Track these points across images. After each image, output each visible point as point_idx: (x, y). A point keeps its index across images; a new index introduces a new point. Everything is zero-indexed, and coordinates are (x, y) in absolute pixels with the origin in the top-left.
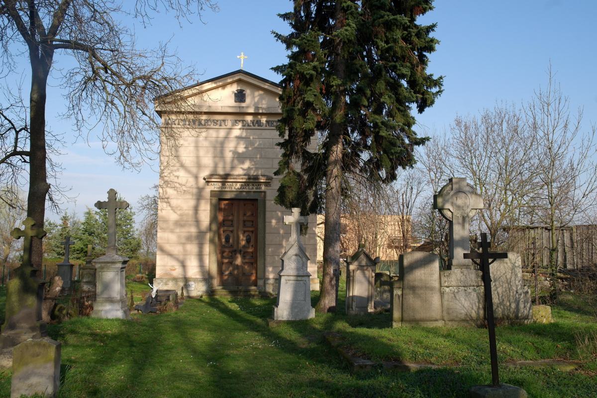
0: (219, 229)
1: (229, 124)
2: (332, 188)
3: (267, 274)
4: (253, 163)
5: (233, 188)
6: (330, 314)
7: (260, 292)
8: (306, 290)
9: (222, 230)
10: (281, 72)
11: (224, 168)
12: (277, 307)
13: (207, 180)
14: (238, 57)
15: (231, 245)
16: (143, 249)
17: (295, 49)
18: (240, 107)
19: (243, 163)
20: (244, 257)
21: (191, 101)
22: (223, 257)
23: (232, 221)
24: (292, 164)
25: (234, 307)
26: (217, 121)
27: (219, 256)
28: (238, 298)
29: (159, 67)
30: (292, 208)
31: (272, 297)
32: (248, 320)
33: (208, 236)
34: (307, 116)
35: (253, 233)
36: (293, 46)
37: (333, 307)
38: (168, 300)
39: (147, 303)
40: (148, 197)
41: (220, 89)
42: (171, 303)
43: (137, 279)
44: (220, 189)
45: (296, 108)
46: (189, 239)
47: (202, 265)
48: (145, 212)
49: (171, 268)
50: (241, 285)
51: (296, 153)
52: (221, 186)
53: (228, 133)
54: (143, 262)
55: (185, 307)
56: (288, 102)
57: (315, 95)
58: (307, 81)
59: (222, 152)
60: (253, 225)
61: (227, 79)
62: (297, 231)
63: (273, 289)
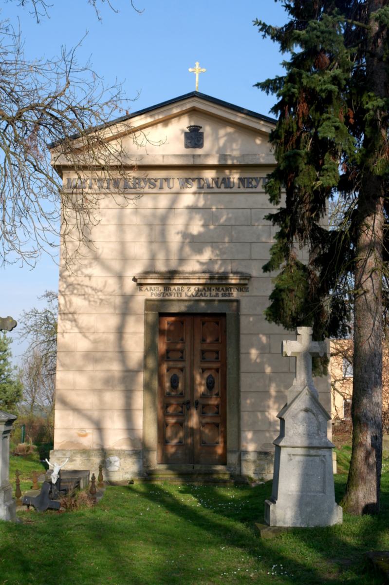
0: (159, 365)
1: (176, 185)
2: (365, 292)
3: (244, 443)
4: (218, 252)
5: (183, 294)
6: (368, 517)
7: (232, 476)
8: (324, 475)
9: (164, 367)
10: (274, 90)
11: (167, 260)
12: (275, 503)
13: (139, 281)
14: (190, 70)
15: (181, 394)
16: (26, 400)
17: (298, 49)
18: (194, 156)
19: (200, 251)
20: (202, 414)
21: (114, 146)
22: (166, 414)
23: (182, 352)
24: (295, 250)
25: (190, 500)
26: (156, 180)
27: (161, 413)
28: (194, 486)
29: (62, 89)
30: (298, 328)
31: (253, 485)
32: (220, 526)
33: (141, 377)
34: (323, 164)
36: (293, 45)
37: (373, 504)
38: (78, 487)
39: (43, 494)
40: (35, 313)
41: (160, 125)
42: (83, 493)
43: (20, 451)
44: (161, 297)
45: (303, 152)
46: (108, 383)
47: (130, 429)
48: (31, 337)
49: (80, 432)
50: (198, 463)
51: (301, 231)
52: (162, 291)
53: (174, 202)
54: (26, 422)
55: (107, 500)
56: (286, 142)
57: (337, 128)
58: (320, 102)
59: (163, 233)
60: (217, 358)
61: (173, 108)
62: (307, 367)
63: (255, 470)
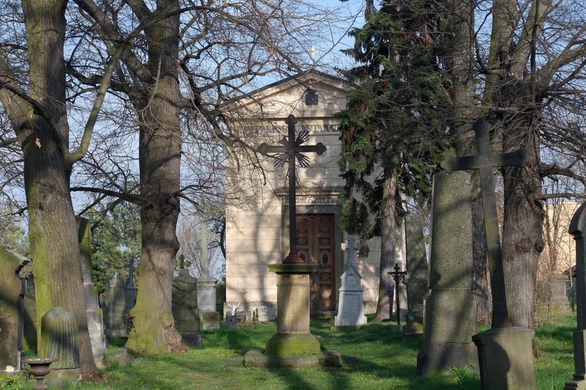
35: (330, 251)
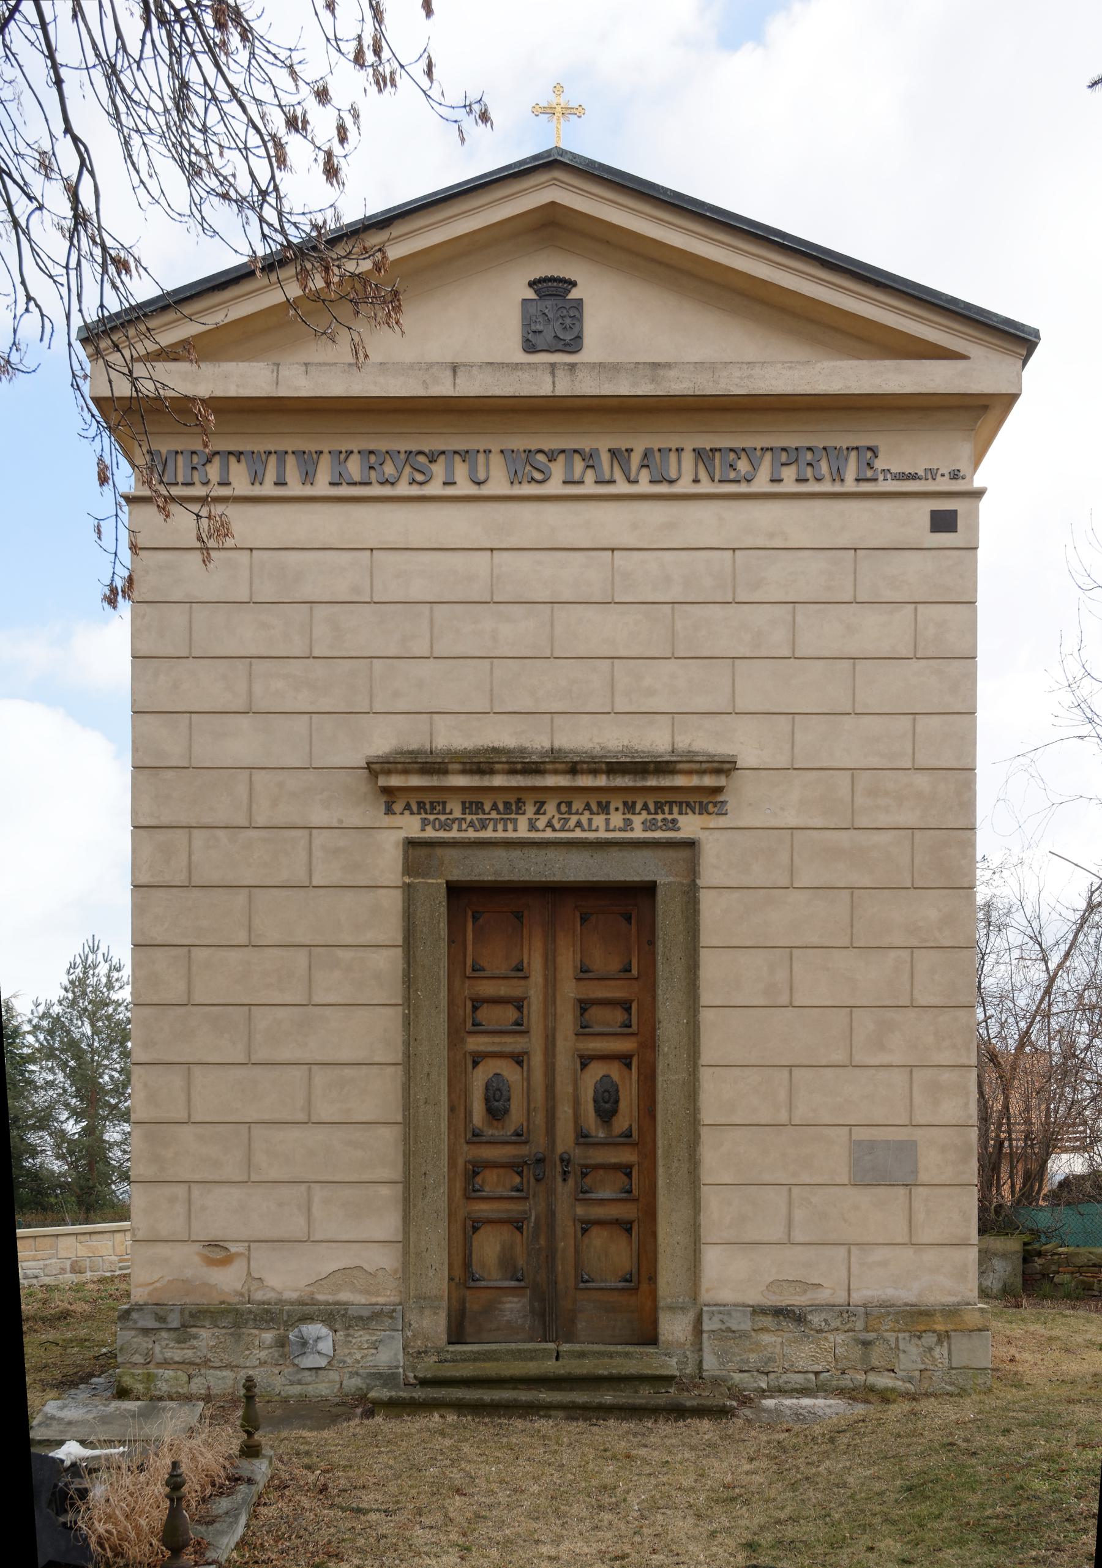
23: (520, 1008)
